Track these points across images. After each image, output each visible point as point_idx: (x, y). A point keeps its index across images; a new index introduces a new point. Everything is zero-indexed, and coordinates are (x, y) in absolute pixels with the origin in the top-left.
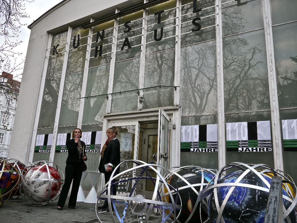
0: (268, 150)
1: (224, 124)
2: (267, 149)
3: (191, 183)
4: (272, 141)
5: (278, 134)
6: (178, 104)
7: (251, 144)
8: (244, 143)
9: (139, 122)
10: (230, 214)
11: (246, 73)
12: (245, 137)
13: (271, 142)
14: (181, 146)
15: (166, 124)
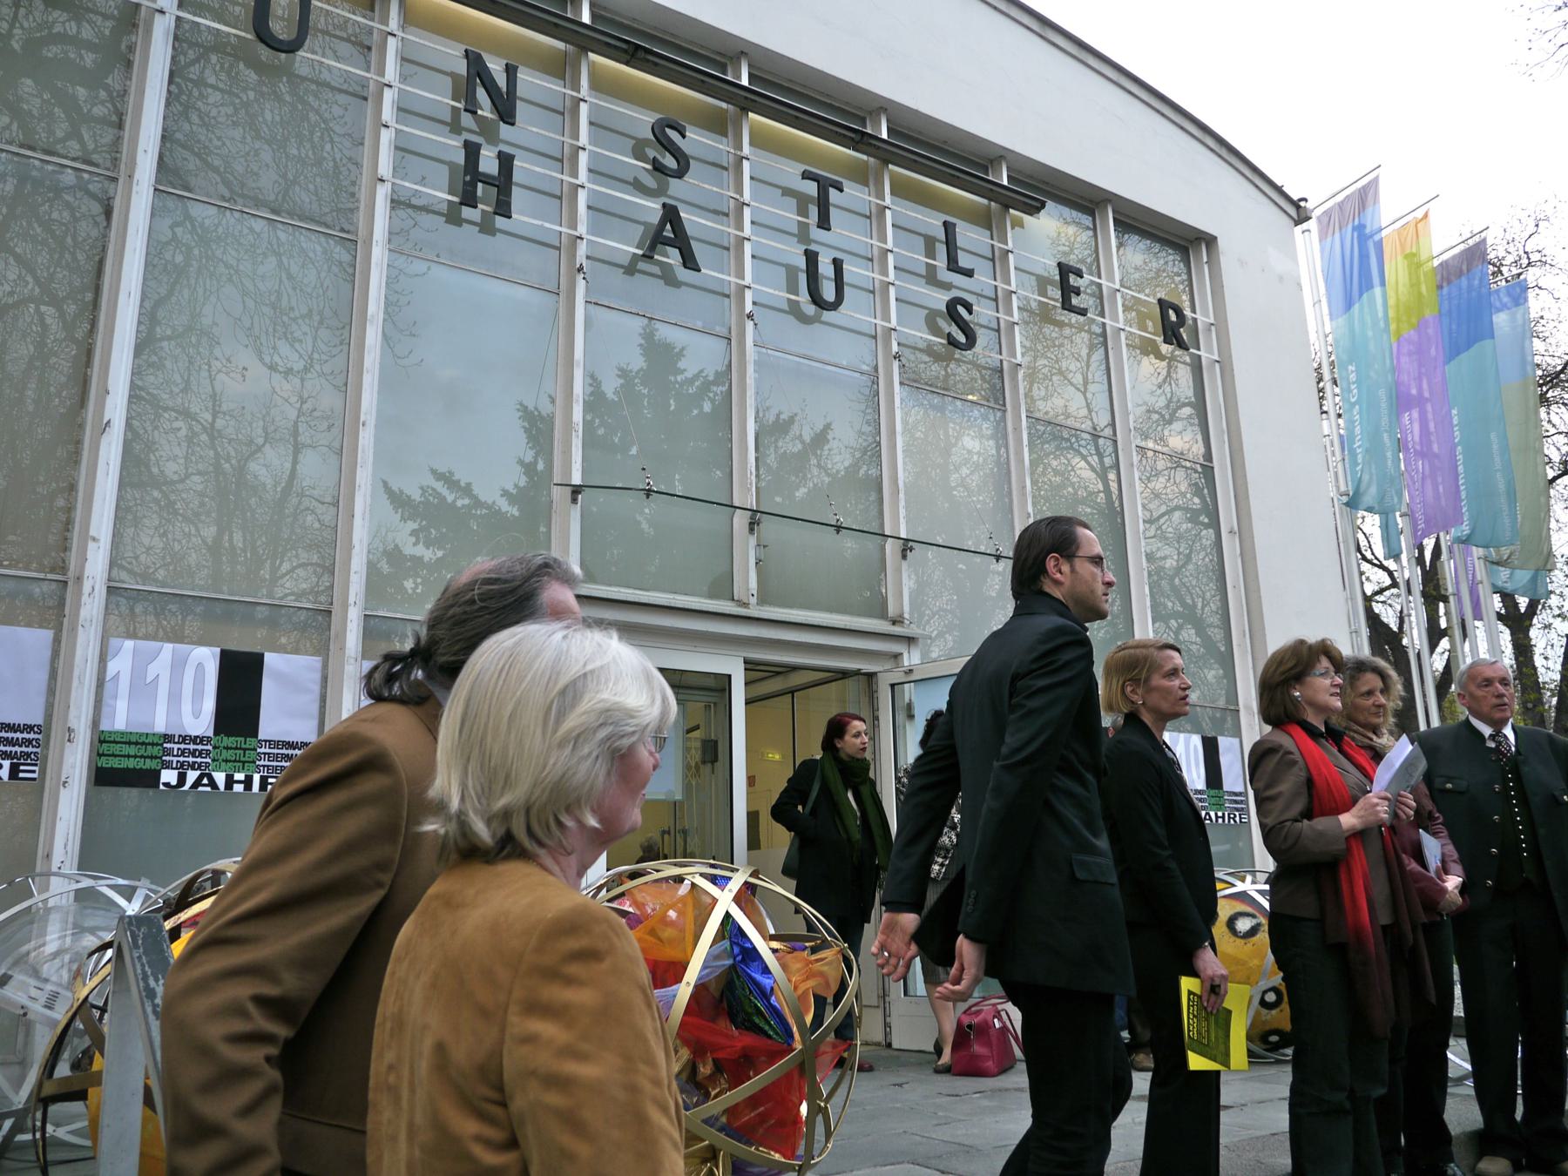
0: (21, 775)
8: (192, 747)
12: (199, 717)
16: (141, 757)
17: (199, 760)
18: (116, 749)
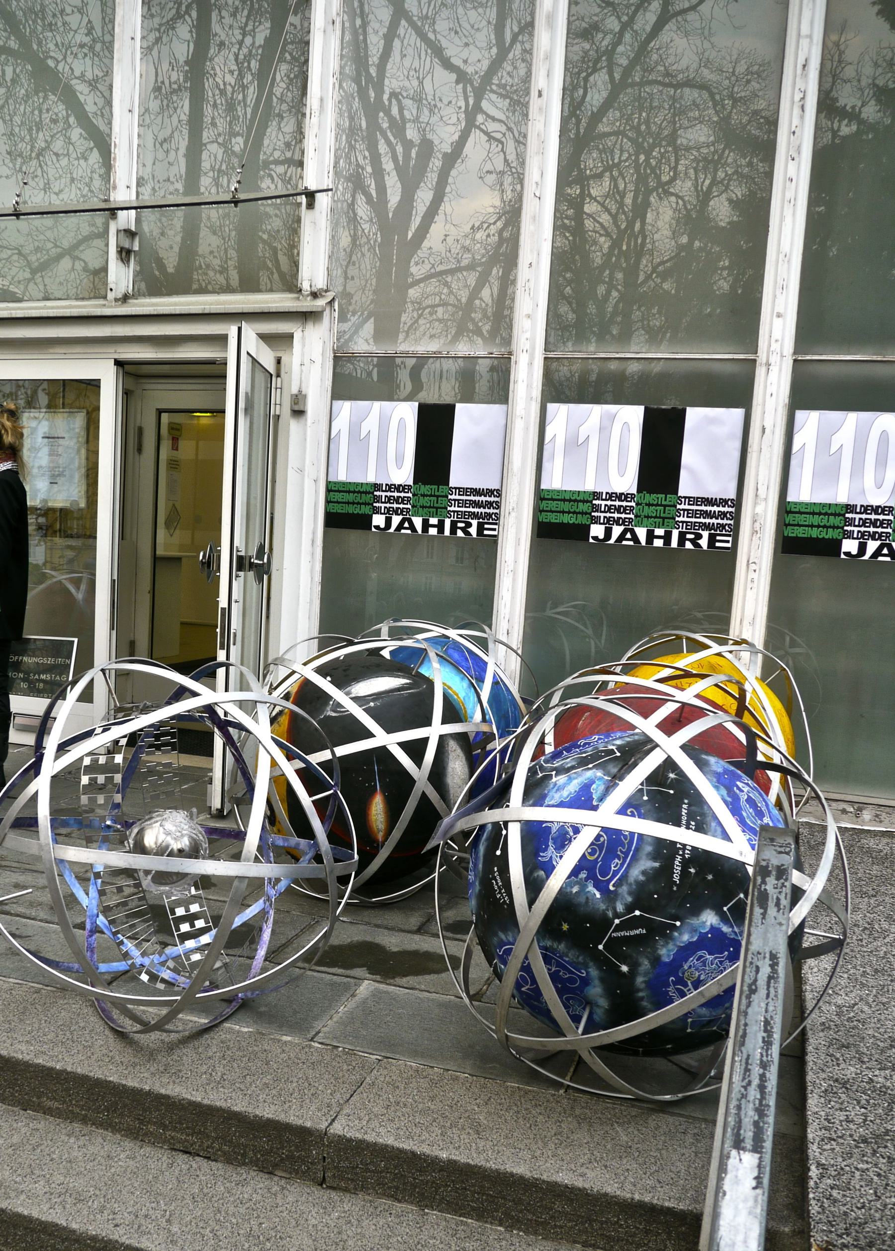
1: (535, 408)
2: (712, 540)
3: (390, 729)
4: (737, 503)
5: (770, 473)
6: (320, 283)
7: (648, 511)
8: (617, 503)
9: (118, 363)
10: (565, 927)
11: (642, 50)
13: (733, 510)
14: (328, 502)
15: (256, 390)
16: (574, 513)
17: (623, 516)
18: (800, 519)
